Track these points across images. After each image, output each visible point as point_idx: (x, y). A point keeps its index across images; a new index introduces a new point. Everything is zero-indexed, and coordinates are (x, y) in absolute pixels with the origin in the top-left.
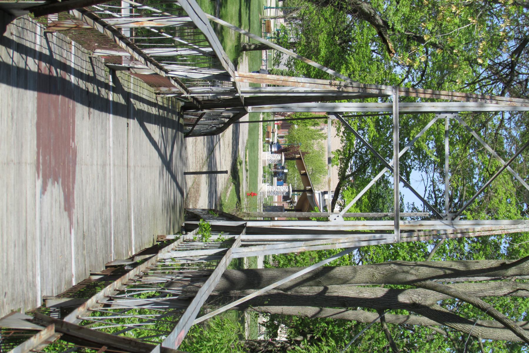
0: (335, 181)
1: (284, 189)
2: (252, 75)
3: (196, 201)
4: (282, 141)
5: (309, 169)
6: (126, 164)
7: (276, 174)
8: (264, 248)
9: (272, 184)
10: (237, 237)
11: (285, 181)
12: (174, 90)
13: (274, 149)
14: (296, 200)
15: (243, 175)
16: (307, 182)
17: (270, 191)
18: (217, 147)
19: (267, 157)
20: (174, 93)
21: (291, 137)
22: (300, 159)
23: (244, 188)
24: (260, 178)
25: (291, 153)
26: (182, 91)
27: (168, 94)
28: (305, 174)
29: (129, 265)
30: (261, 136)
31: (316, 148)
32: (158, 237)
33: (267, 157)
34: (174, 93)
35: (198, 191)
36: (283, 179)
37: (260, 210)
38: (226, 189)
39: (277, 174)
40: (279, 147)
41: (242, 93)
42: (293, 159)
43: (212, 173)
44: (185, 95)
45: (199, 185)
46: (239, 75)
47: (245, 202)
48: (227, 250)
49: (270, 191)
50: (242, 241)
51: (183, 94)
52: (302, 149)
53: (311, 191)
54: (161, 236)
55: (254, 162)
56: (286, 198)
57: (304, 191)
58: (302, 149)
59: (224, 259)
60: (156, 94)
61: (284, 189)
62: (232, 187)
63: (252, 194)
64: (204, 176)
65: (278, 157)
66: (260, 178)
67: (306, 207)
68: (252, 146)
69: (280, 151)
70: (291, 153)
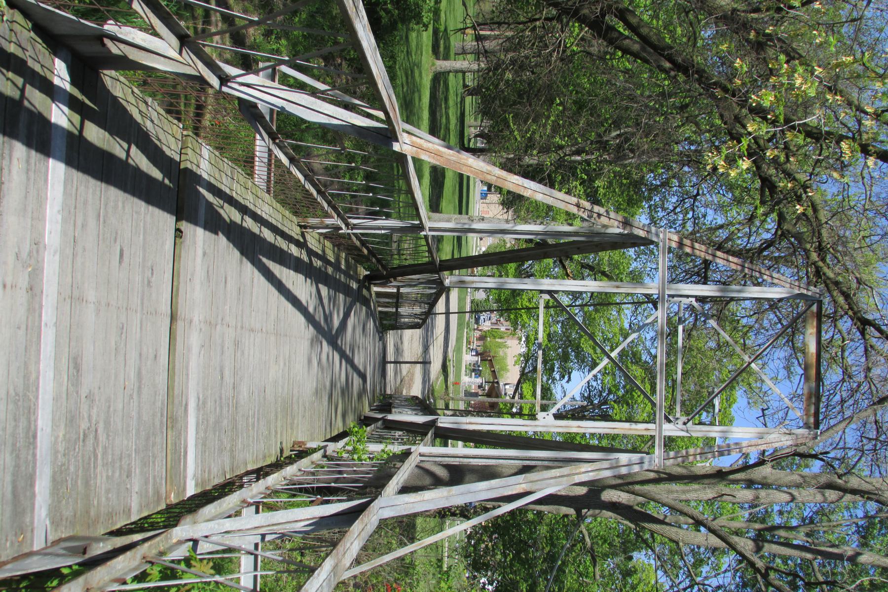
0: (517, 376)
1: (479, 380)
2: (438, 150)
3: (410, 387)
4: (479, 349)
5: (497, 367)
6: (166, 309)
7: (474, 370)
8: (449, 492)
9: (471, 377)
10: (413, 448)
11: (480, 375)
12: (328, 221)
13: (474, 353)
14: (487, 388)
15: (451, 370)
16: (495, 377)
17: (470, 382)
18: (431, 347)
19: (469, 358)
20: (327, 227)
21: (485, 346)
22: (491, 360)
23: (451, 378)
24: (463, 372)
25: (485, 356)
26: (340, 223)
27: (319, 228)
28: (494, 371)
29: (76, 564)
30: (465, 344)
31: (501, 353)
32: (295, 443)
33: (469, 358)
34: (327, 227)
35: (412, 380)
36: (478, 374)
37: (462, 395)
38: (437, 379)
39: (475, 370)
40: (477, 352)
41: (431, 229)
42: (486, 360)
43: (426, 363)
44: (344, 230)
45: (413, 375)
46: (413, 142)
47: (451, 388)
48: (367, 504)
49: (470, 382)
50: (421, 455)
51: (341, 229)
52: (492, 354)
53: (498, 383)
54: (300, 442)
55: (459, 361)
56: (480, 387)
57: (493, 382)
58: (492, 354)
59: (357, 527)
60: (301, 226)
61: (479, 380)
62: (442, 378)
63: (457, 384)
64: (419, 365)
65: (476, 358)
66: (463, 372)
67: (494, 394)
68: (458, 350)
69: (477, 354)
70: (485, 356)
